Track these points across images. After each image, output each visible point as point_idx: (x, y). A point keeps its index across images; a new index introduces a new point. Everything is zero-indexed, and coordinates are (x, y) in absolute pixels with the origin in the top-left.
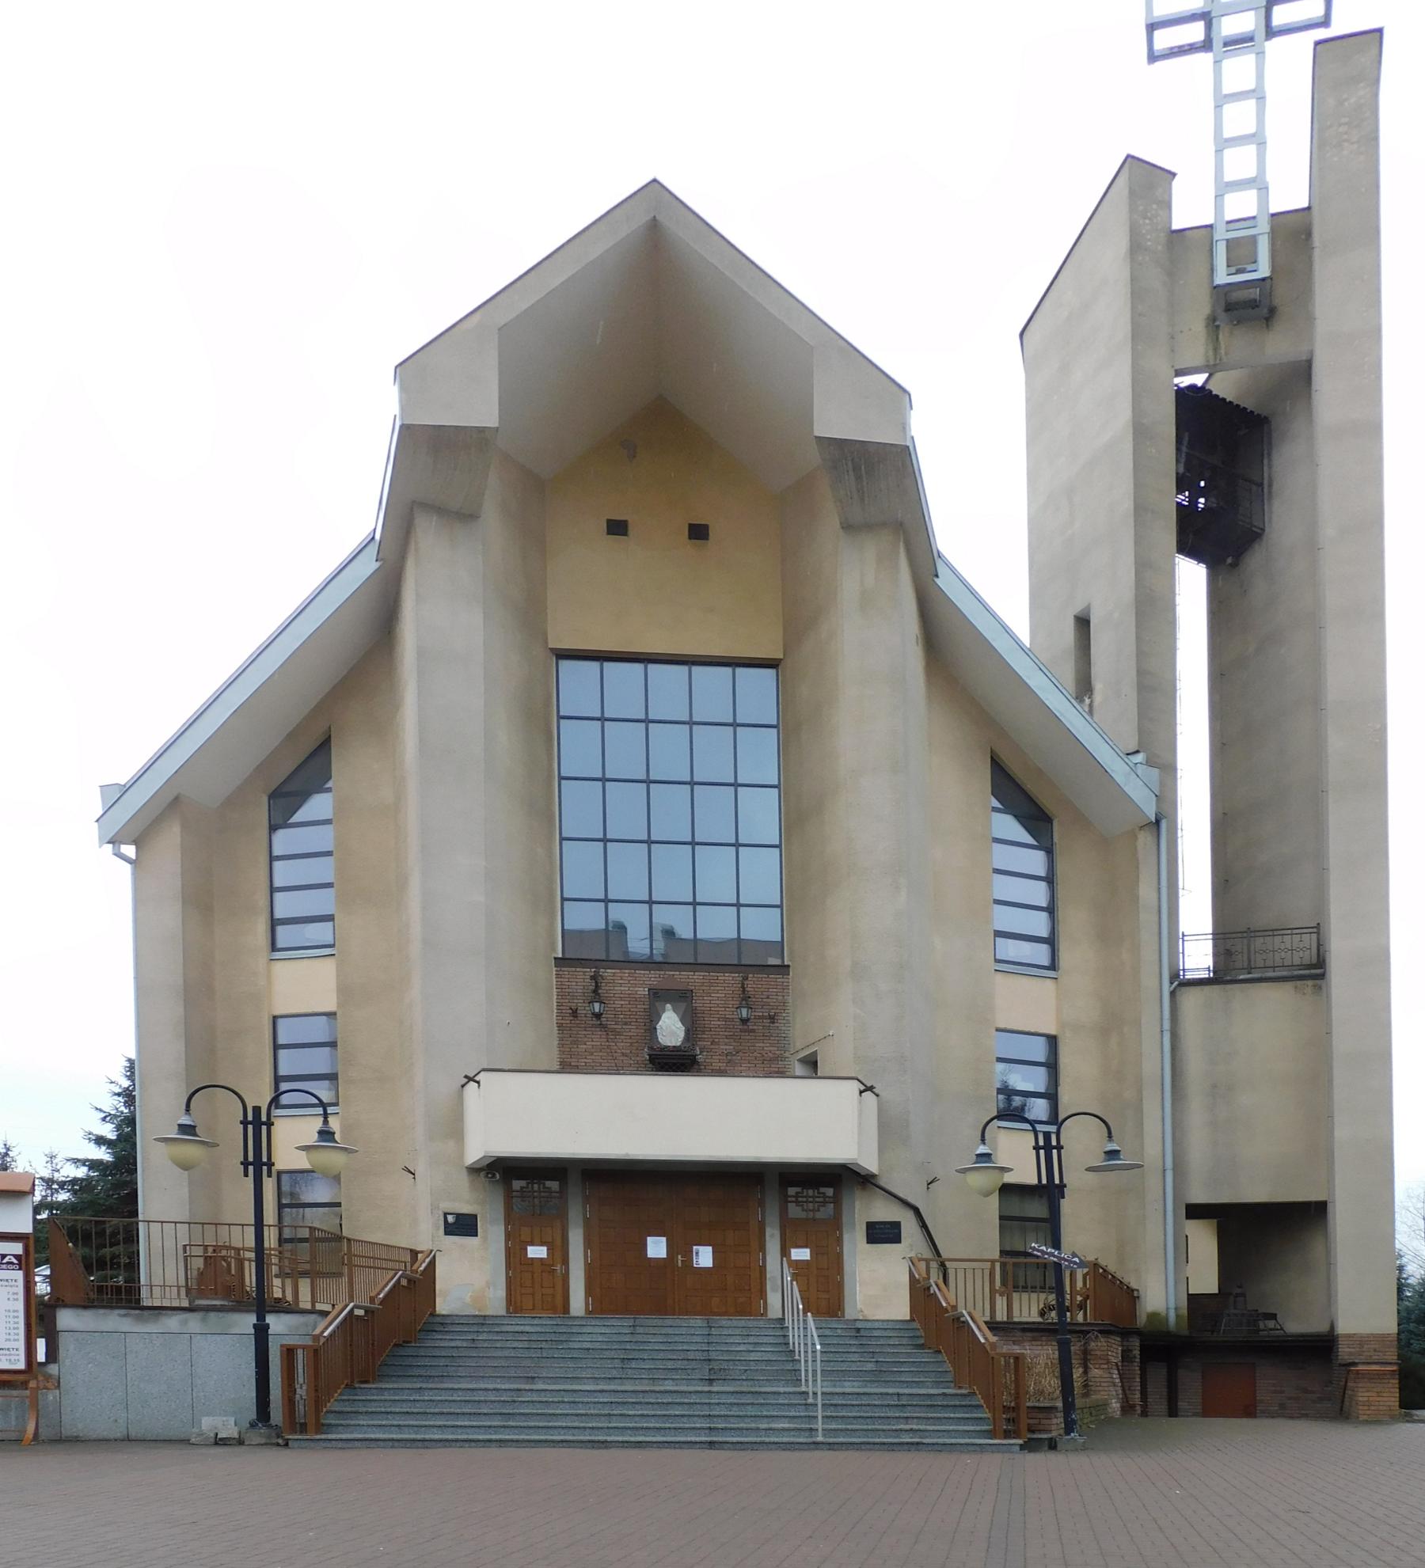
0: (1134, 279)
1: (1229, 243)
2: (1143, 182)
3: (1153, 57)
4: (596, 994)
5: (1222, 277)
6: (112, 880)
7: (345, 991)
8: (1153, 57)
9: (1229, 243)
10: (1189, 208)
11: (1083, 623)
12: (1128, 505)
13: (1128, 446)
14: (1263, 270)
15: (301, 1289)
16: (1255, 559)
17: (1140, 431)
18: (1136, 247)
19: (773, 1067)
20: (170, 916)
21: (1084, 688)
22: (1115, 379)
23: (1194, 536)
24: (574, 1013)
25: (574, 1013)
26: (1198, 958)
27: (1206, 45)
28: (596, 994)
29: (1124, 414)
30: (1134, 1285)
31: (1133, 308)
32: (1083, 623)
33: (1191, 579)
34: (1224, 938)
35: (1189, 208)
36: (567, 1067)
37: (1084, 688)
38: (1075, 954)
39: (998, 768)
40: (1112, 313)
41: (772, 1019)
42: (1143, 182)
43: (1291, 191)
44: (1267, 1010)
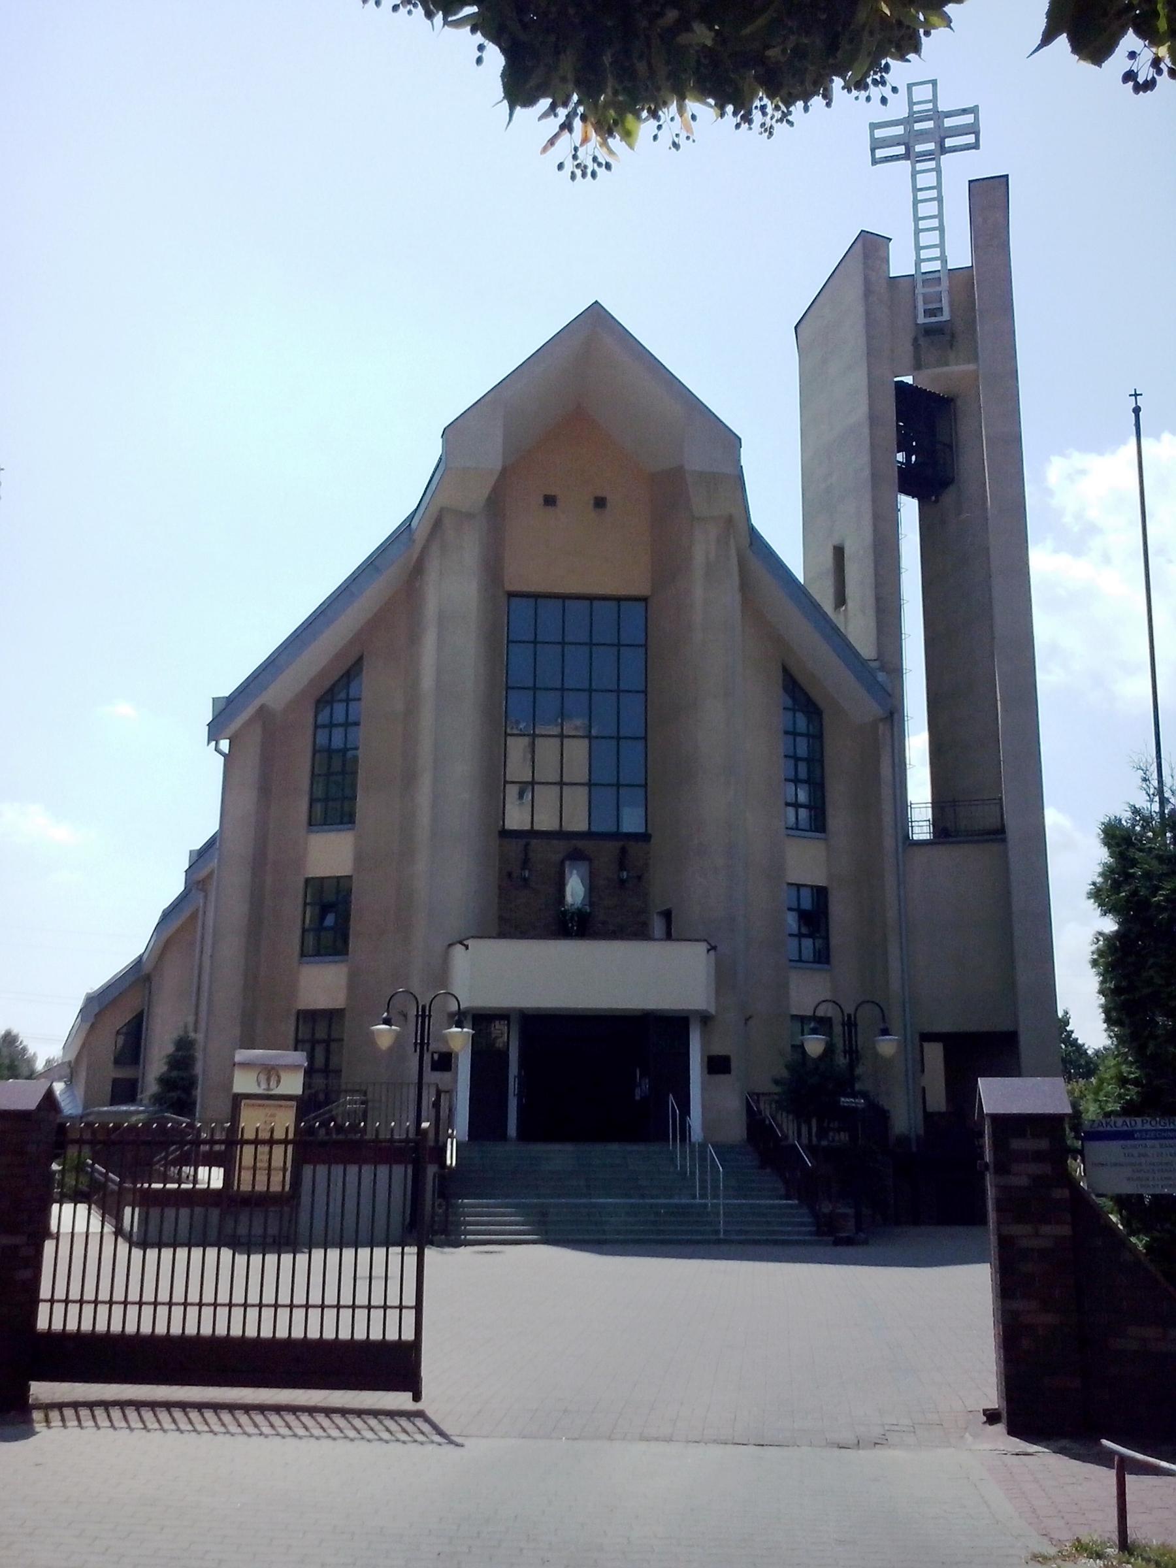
0: (868, 314)
1: (924, 295)
2: (870, 247)
3: (875, 162)
4: (525, 863)
5: (921, 320)
6: (208, 766)
7: (359, 859)
8: (875, 162)
9: (924, 295)
10: (900, 264)
11: (839, 552)
12: (867, 473)
13: (866, 431)
14: (946, 316)
15: (323, 1061)
16: (948, 497)
17: (873, 419)
18: (868, 292)
19: (640, 932)
20: (248, 800)
21: (841, 600)
22: (858, 379)
23: (910, 482)
24: (510, 875)
25: (510, 875)
26: (921, 830)
27: (906, 156)
28: (525, 863)
29: (862, 409)
30: (886, 1107)
31: (867, 332)
32: (839, 552)
33: (909, 508)
34: (939, 803)
35: (900, 264)
36: (502, 935)
37: (841, 600)
38: (838, 818)
39: (786, 671)
40: (853, 334)
41: (639, 878)
42: (870, 247)
43: (960, 255)
44: (967, 858)
